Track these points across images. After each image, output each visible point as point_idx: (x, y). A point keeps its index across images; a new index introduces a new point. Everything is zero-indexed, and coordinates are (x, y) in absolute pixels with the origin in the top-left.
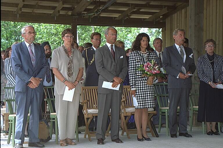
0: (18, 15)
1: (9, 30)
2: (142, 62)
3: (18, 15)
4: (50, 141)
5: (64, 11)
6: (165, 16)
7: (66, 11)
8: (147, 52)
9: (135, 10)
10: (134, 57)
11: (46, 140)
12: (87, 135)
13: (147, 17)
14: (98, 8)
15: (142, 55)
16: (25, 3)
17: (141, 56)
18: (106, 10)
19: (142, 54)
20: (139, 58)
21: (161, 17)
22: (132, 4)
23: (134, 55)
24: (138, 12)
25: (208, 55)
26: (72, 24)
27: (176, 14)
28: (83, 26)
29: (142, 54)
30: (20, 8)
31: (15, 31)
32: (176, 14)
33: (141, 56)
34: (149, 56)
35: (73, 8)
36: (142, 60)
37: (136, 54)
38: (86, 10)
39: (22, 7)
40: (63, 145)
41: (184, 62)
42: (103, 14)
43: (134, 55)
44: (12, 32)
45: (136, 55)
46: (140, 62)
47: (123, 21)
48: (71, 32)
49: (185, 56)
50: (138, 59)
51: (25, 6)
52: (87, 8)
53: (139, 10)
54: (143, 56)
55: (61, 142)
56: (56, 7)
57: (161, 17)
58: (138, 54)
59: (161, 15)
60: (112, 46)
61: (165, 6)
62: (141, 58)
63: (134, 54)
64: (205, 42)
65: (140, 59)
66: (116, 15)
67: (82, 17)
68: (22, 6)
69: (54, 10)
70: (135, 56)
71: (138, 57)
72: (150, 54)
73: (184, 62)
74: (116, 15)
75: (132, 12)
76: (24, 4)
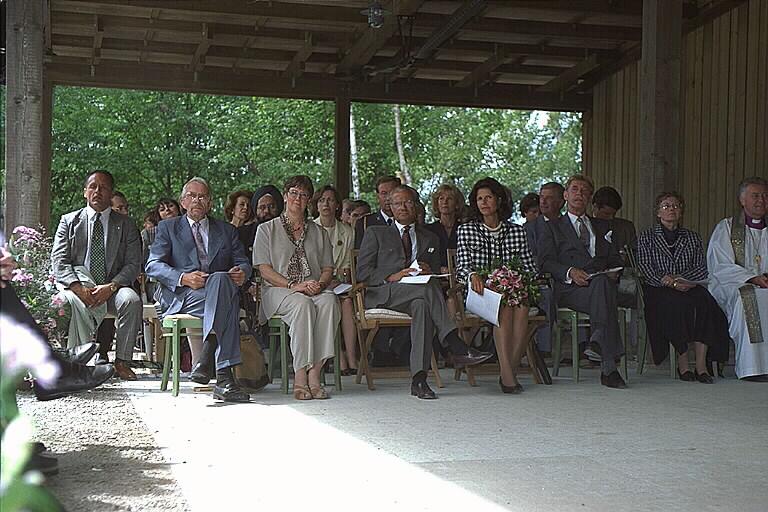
0: (196, 74)
1: (174, 120)
2: (485, 253)
3: (196, 74)
4: (269, 386)
5: (317, 64)
6: (592, 78)
7: (323, 65)
8: (502, 227)
9: (508, 61)
10: (467, 237)
11: (257, 382)
12: (364, 377)
13: (540, 81)
14: (407, 55)
15: (486, 234)
16: (216, 43)
17: (484, 237)
18: (428, 62)
19: (489, 232)
20: (480, 241)
21: (580, 81)
22: (500, 45)
23: (466, 232)
24: (518, 68)
25: (664, 229)
26: (337, 99)
27: (620, 74)
28: (370, 105)
29: (489, 232)
30: (201, 57)
31: (189, 122)
32: (622, 72)
33: (484, 237)
34: (504, 238)
35: (340, 57)
36: (484, 247)
37: (473, 230)
38: (376, 61)
39: (207, 54)
40: (302, 396)
41: (593, 255)
42: (422, 73)
43: (466, 232)
44: (181, 126)
45: (471, 232)
46: (481, 253)
47: (476, 89)
48: (305, 187)
49: (593, 240)
50: (478, 243)
51: (214, 51)
52: (378, 54)
53: (522, 59)
54: (489, 237)
55: (296, 390)
56: (296, 52)
57: (580, 81)
58: (479, 230)
59: (579, 75)
60: (407, 230)
61: (591, 51)
62: (484, 242)
63: (468, 229)
64: (660, 197)
65: (480, 245)
66: (458, 76)
67: (366, 79)
68: (206, 50)
69: (288, 62)
70: (469, 234)
71: (477, 238)
72: (508, 230)
73: (593, 255)
74: (458, 76)
75: (500, 66)
76: (211, 46)
